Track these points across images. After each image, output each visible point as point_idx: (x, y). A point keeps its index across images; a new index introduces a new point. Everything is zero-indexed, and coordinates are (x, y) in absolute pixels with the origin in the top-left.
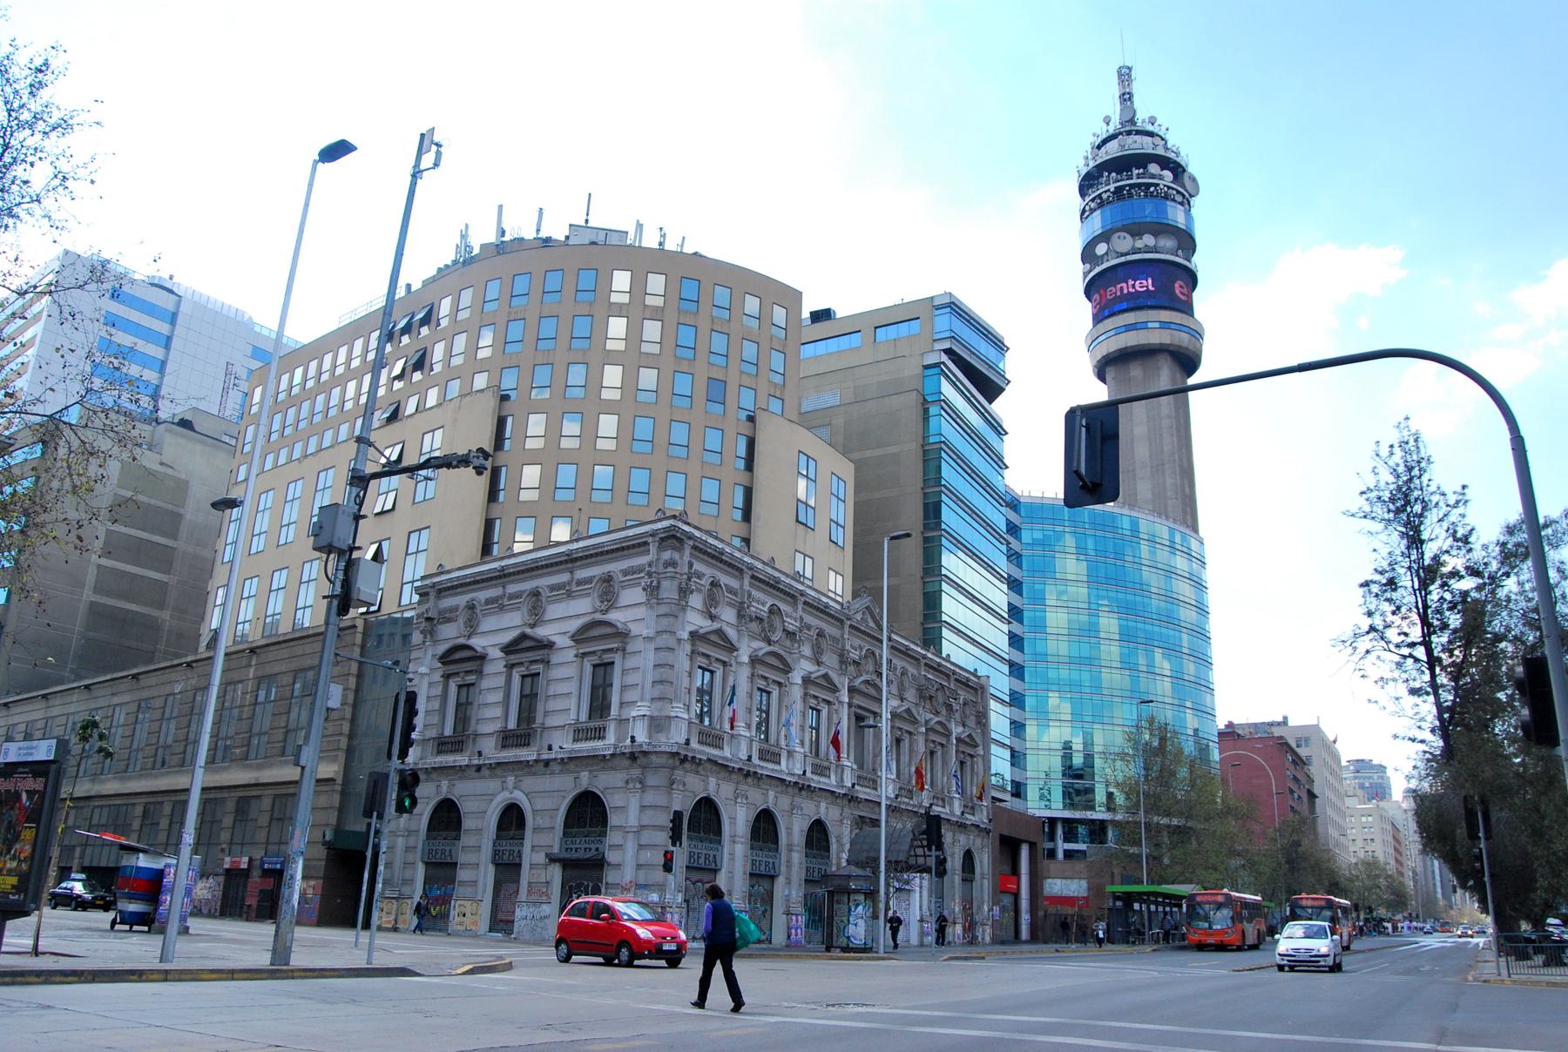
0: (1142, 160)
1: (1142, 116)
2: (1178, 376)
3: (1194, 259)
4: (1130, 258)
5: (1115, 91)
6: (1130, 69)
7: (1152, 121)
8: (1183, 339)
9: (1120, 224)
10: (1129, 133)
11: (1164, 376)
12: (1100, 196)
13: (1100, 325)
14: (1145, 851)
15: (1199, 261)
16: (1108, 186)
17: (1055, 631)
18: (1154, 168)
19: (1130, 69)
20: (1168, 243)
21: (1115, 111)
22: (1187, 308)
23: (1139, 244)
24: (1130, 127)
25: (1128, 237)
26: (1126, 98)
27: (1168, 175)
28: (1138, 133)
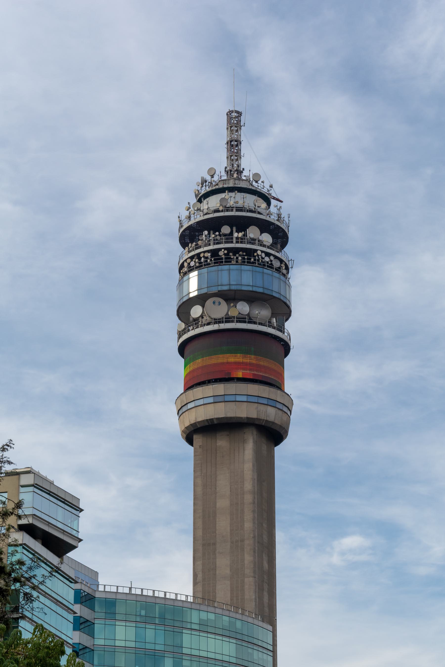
0: (241, 224)
1: (250, 164)
2: (264, 447)
3: (288, 325)
4: (223, 326)
5: (224, 136)
6: (239, 114)
7: (257, 177)
8: (270, 414)
9: (214, 290)
10: (231, 190)
11: (249, 445)
12: (198, 255)
13: (190, 392)
14: (224, 260)
15: (294, 328)
16: (206, 245)
17: (122, 644)
18: (253, 232)
19: (239, 114)
20: (263, 313)
21: (220, 162)
22: (278, 385)
23: (233, 313)
24: (235, 182)
25: (224, 304)
26: (234, 146)
27: (267, 238)
28: (241, 190)
